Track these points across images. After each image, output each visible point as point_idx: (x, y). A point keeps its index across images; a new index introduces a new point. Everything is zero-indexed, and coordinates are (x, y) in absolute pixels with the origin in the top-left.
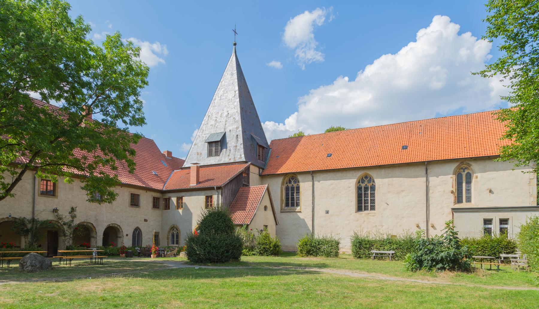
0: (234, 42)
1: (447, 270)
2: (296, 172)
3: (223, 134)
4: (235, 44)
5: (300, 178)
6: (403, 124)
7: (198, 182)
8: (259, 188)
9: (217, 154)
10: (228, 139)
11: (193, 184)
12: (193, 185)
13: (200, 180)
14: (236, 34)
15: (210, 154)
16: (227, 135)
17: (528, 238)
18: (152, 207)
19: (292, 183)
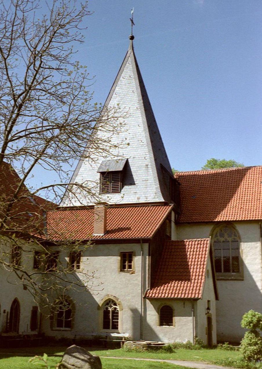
0: (131, 35)
1: (236, 350)
2: (233, 221)
3: (124, 162)
4: (132, 38)
5: (240, 229)
6: (254, 168)
7: (107, 232)
8: (197, 243)
9: (116, 191)
10: (133, 169)
11: (99, 234)
12: (99, 235)
13: (109, 228)
14: (133, 25)
15: (104, 190)
16: (130, 164)
17: (57, 301)
18: (119, 270)
19: (226, 236)
